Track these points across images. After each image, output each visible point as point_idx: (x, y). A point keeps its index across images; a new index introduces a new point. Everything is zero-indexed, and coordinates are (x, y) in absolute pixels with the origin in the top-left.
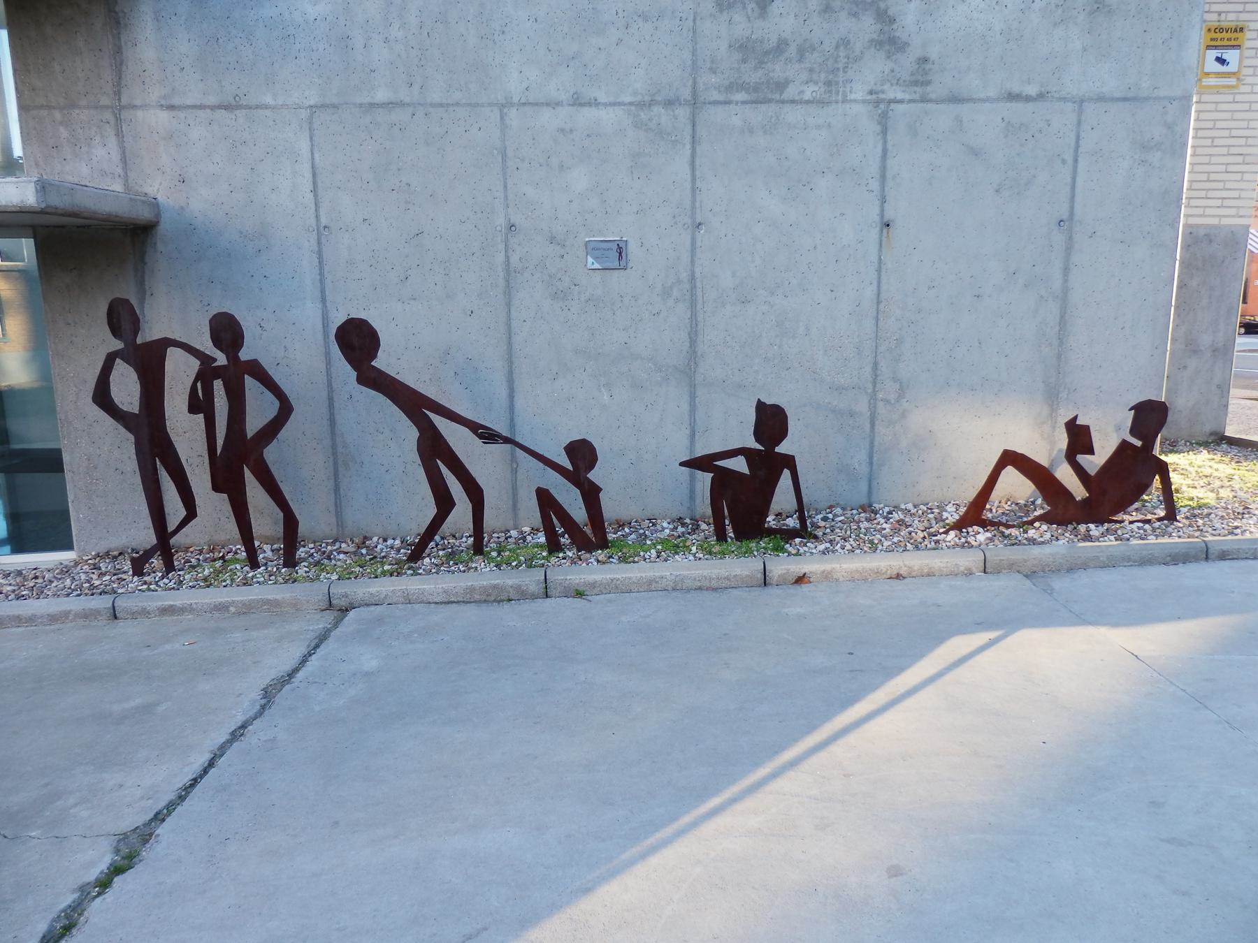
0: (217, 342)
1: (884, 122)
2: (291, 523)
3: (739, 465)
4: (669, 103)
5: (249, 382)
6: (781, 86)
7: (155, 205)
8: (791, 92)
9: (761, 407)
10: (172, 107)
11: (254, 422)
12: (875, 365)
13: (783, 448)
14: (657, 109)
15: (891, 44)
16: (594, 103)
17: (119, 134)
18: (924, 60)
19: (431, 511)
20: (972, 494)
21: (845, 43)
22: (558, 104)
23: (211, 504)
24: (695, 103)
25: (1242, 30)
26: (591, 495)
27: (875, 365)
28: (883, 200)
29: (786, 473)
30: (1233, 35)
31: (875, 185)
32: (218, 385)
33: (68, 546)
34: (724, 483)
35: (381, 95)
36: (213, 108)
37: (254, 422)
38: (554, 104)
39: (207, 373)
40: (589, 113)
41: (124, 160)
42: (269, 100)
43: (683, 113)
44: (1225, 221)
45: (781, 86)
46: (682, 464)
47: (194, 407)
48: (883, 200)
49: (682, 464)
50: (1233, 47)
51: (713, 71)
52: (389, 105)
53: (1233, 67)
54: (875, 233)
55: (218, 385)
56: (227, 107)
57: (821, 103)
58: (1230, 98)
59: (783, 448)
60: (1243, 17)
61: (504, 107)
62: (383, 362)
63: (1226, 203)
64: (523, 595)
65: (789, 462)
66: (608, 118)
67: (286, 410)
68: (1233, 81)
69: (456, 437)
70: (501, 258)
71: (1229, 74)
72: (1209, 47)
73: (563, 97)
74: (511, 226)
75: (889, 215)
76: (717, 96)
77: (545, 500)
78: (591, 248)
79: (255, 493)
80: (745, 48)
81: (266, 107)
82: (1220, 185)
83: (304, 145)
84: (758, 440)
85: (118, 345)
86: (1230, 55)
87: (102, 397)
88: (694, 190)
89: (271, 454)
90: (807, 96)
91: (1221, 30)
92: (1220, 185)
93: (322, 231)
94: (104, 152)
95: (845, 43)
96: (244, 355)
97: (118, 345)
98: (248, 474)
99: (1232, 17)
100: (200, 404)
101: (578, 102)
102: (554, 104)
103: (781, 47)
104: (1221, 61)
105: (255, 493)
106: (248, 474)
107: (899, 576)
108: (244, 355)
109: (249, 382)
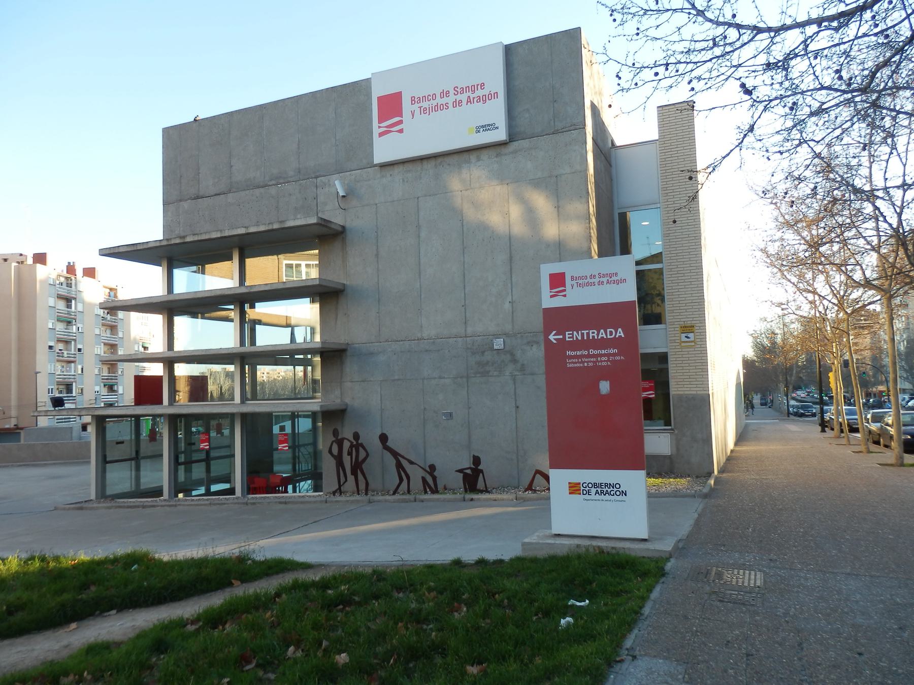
0: (354, 439)
1: (514, 381)
2: (367, 484)
3: (469, 471)
4: (462, 377)
5: (361, 449)
6: (488, 372)
7: (347, 405)
8: (491, 374)
9: (474, 456)
10: (352, 382)
11: (361, 458)
12: (517, 446)
13: (480, 467)
14: (459, 379)
15: (514, 361)
16: (444, 378)
17: (341, 388)
18: (523, 365)
19: (398, 481)
20: (528, 483)
21: (503, 361)
22: (436, 378)
23: (351, 478)
24: (468, 377)
25: (693, 327)
26: (434, 479)
27: (517, 446)
28: (516, 400)
29: (481, 474)
30: (690, 329)
31: (513, 397)
32: (354, 449)
33: (322, 491)
34: (466, 476)
35: (396, 377)
36: (361, 382)
37: (361, 458)
38: (435, 378)
39: (352, 446)
40: (443, 380)
41: (341, 394)
42: (372, 379)
43: (465, 380)
44: (698, 392)
45: (488, 372)
46: (456, 471)
47: (348, 455)
48: (516, 400)
49: (456, 471)
50: (691, 332)
51: (472, 369)
52: (398, 380)
53: (692, 339)
54: (514, 408)
55: (354, 449)
56: (363, 381)
57: (498, 376)
58: (693, 349)
59: (480, 467)
60: (693, 322)
61: (423, 379)
62: (389, 444)
63: (698, 386)
64: (410, 501)
65: (482, 471)
66: (447, 381)
67: (368, 455)
68: (693, 344)
69: (405, 463)
70: (422, 417)
71: (689, 342)
72: (682, 333)
73: (437, 376)
74: (425, 409)
75: (518, 405)
76: (473, 375)
77: (424, 479)
78: (444, 414)
79: (360, 476)
80: (479, 363)
81: (371, 381)
82: (695, 380)
83: (379, 390)
84: (474, 465)
85: (334, 439)
86: (691, 335)
87: (330, 452)
88: (468, 399)
89: (364, 466)
90: (495, 375)
91: (686, 327)
92: (695, 380)
93: (382, 410)
94: (337, 392)
95: (503, 361)
96: (360, 442)
97: (334, 439)
98: (359, 471)
99: (689, 322)
100: (350, 454)
101: (440, 378)
102: (435, 378)
103: (488, 363)
104: (687, 337)
105: (360, 476)
106: (359, 471)
107: (495, 500)
108: (360, 442)
109: (361, 449)
